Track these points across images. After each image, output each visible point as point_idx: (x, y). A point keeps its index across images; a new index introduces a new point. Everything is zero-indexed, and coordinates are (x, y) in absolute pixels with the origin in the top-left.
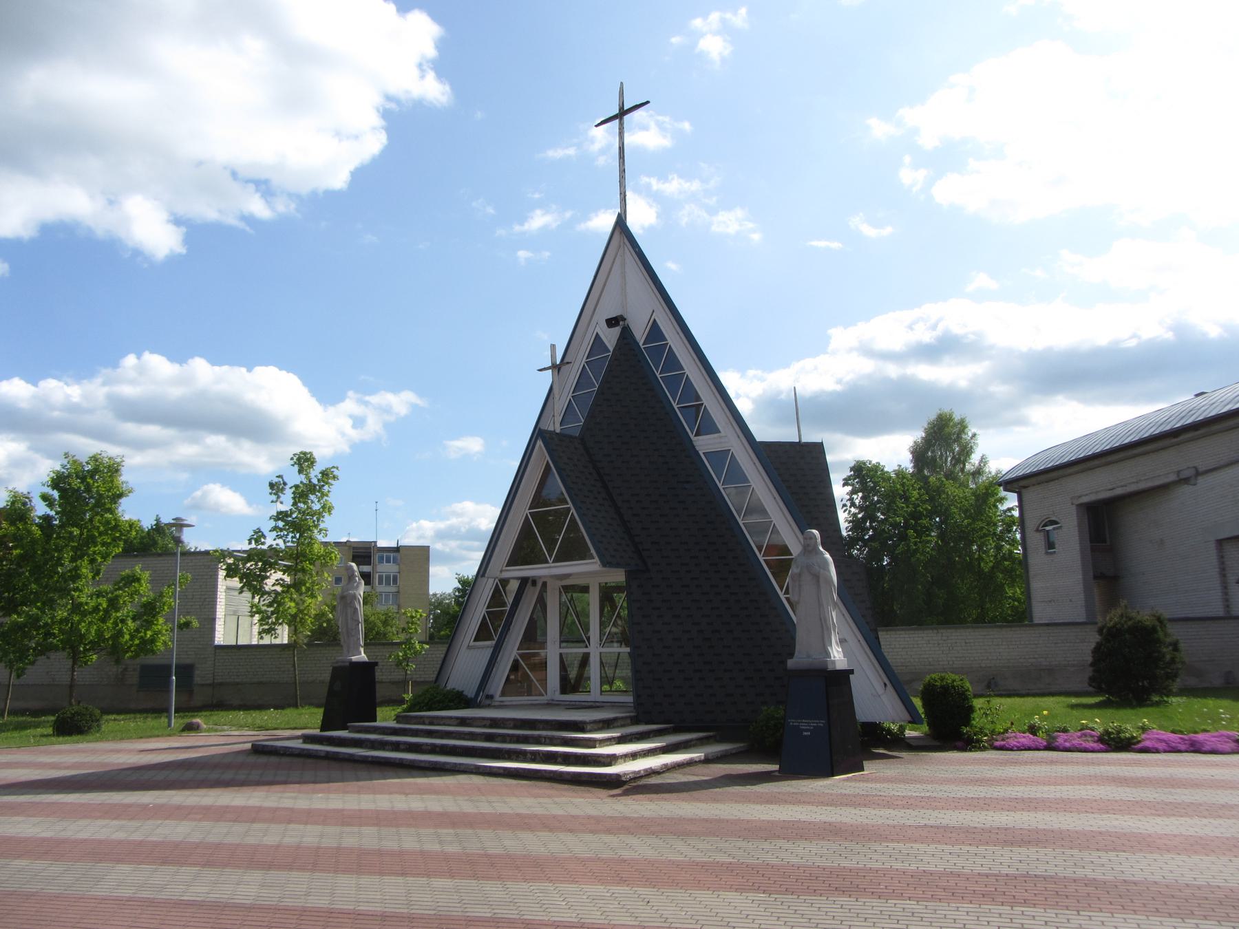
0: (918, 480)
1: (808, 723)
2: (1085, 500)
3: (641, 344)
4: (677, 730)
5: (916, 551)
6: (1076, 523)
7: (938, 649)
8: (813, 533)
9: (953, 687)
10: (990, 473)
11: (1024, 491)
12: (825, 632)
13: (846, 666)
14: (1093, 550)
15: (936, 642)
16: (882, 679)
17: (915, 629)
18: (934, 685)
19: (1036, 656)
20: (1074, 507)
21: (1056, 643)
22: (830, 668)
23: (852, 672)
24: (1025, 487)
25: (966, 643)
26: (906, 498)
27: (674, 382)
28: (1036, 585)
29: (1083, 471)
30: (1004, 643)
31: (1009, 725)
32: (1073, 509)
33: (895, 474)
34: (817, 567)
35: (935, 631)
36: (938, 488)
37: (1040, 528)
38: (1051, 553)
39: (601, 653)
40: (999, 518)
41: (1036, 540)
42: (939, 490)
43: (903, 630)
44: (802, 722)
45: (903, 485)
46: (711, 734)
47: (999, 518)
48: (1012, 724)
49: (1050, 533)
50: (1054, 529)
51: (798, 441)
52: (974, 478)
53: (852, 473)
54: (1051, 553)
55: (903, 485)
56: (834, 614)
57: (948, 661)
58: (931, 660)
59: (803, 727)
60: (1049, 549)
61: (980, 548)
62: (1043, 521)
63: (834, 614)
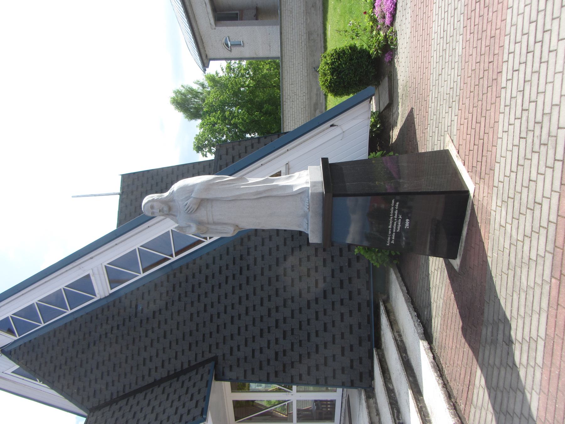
0: (205, 117)
1: (393, 219)
2: (212, 21)
3: (16, 338)
4: (378, 343)
5: (243, 119)
6: (226, 28)
7: (295, 102)
8: (146, 204)
9: (332, 63)
10: (203, 79)
11: (209, 57)
12: (275, 193)
13: (319, 165)
14: (241, 19)
15: (291, 103)
16: (327, 129)
17: (283, 115)
18: (330, 82)
19: (301, 41)
20: (217, 28)
21: (293, 29)
22: (321, 189)
23: (325, 161)
24: (207, 56)
25: (292, 84)
26: (214, 124)
27: (47, 313)
28: (261, 54)
29: (196, 22)
30: (292, 60)
31: (367, 16)
32: (219, 28)
33: (201, 129)
34: (189, 201)
35: (284, 103)
36: (209, 106)
37: (230, 49)
38: (243, 44)
39: (297, 391)
40: (227, 75)
41: (236, 52)
42: (211, 105)
43: (283, 123)
44: (392, 228)
45: (207, 125)
46: (382, 308)
47: (227, 75)
48: (365, 13)
49: (232, 43)
50: (230, 41)
51: (119, 196)
52: (205, 87)
53: (200, 152)
54: (243, 44)
55: (207, 125)
56: (252, 180)
57: (303, 96)
58: (302, 107)
59: (399, 228)
60: (241, 45)
61: (243, 86)
62: (225, 47)
63: (252, 180)
